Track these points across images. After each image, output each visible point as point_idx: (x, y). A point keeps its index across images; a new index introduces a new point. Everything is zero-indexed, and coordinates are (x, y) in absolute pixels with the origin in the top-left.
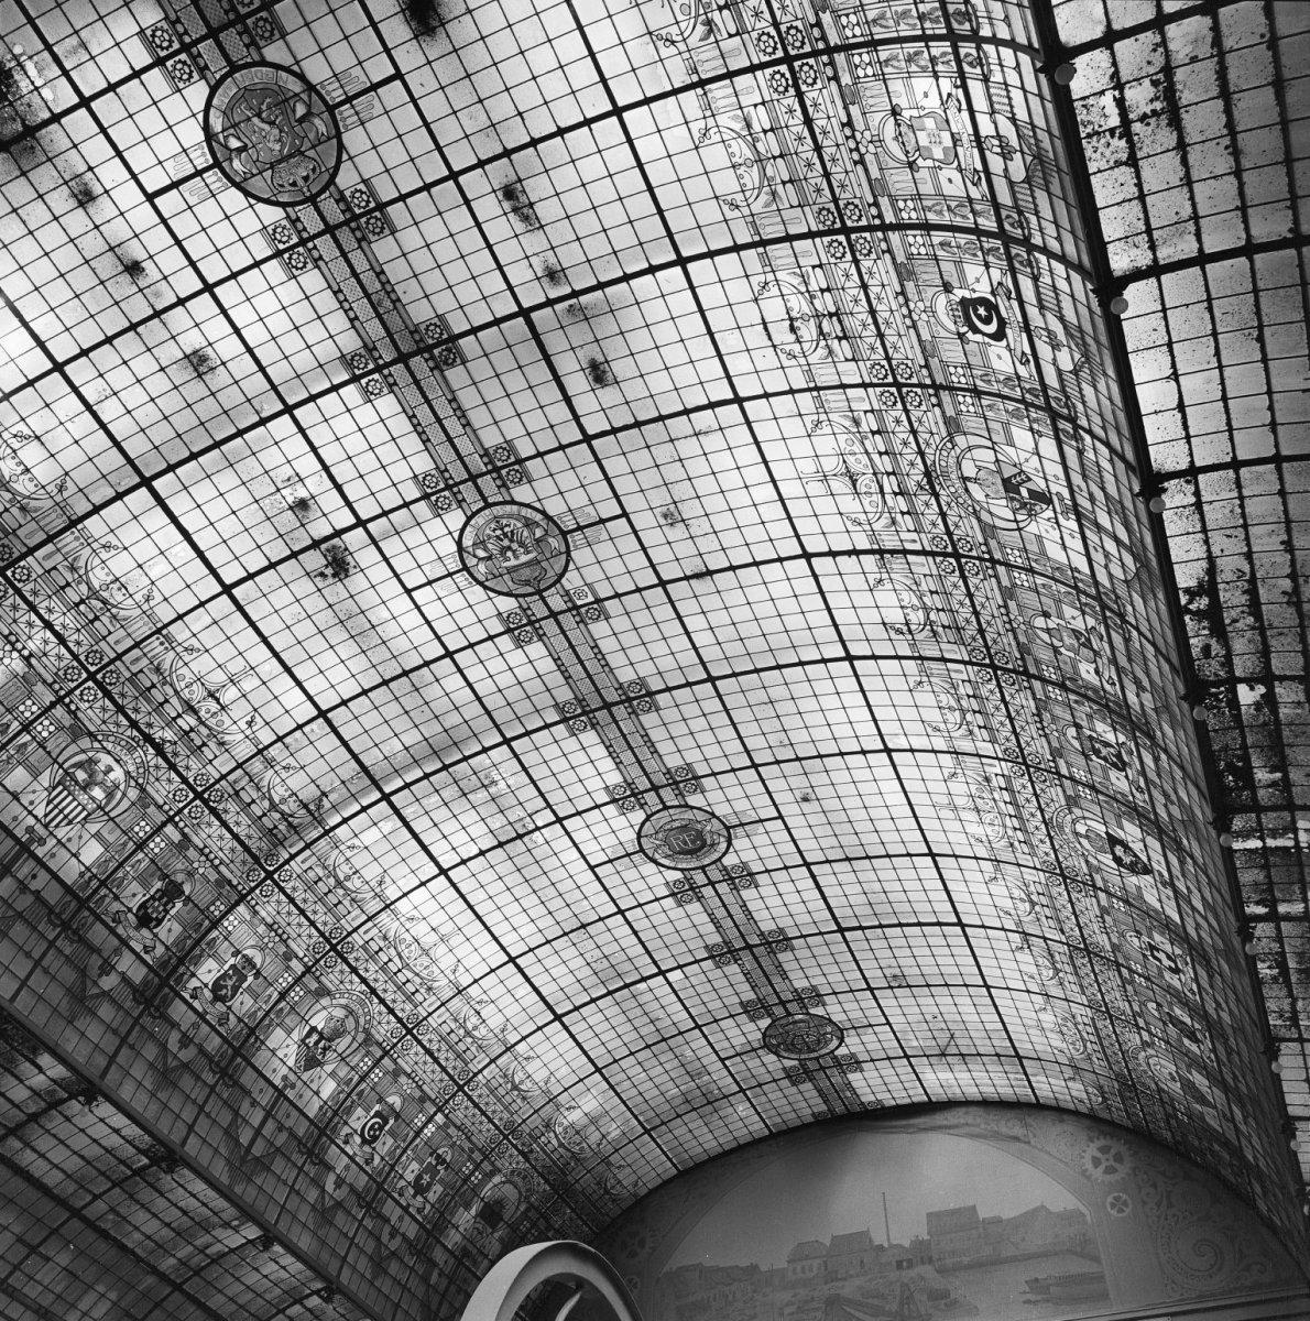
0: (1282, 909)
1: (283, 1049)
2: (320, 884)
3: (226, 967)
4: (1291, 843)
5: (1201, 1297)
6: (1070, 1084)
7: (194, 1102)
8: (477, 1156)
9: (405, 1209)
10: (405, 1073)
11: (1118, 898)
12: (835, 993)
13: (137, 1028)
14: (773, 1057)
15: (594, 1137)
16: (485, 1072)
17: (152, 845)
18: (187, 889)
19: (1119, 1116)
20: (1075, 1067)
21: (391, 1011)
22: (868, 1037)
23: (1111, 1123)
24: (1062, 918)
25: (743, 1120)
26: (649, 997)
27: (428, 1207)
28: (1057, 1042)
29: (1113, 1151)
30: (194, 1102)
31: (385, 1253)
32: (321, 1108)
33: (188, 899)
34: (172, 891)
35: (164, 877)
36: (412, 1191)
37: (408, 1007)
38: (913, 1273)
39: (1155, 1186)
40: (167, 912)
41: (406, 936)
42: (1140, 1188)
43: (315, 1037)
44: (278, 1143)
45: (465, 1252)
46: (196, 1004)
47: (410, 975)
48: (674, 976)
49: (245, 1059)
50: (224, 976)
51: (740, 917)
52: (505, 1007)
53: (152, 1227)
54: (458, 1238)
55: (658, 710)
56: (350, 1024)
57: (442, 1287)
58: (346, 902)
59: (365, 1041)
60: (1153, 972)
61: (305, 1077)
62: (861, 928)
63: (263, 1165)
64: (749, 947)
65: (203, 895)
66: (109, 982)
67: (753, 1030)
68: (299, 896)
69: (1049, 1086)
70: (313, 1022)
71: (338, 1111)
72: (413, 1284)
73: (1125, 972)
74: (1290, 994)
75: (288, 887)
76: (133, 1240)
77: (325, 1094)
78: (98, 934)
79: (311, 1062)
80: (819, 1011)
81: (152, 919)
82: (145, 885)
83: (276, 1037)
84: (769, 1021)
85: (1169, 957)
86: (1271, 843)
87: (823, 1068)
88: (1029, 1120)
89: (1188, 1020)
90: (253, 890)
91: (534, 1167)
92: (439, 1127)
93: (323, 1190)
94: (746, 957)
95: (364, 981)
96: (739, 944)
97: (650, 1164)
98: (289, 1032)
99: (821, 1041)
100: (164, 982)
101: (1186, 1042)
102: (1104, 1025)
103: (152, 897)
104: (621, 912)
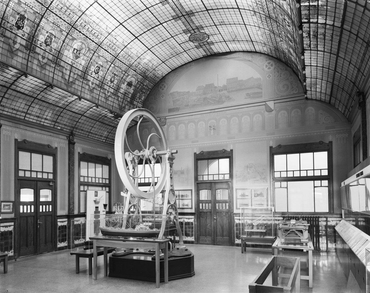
0: (311, 20)
1: (68, 55)
2: (95, 34)
3: (46, 36)
4: (316, 4)
5: (281, 96)
6: (264, 48)
7: (51, 72)
8: (124, 73)
9: (110, 86)
10: (101, 56)
11: (278, 5)
12: (206, 27)
13: (30, 57)
14: (192, 43)
15: (151, 65)
16: (121, 53)
17: (10, 5)
18: (26, 16)
19: (274, 55)
20: (265, 44)
21: (93, 41)
22: (215, 37)
23: (272, 56)
24: (264, 8)
25: (186, 58)
26: (159, 30)
27: (115, 85)
28: (261, 38)
29: (271, 64)
30: (51, 72)
31: (107, 96)
32: (83, 68)
33: (28, 19)
34: (22, 18)
35: (18, 14)
36: (110, 82)
37: (97, 40)
38: (222, 92)
39: (278, 72)
40: (24, 24)
41: (91, 21)
42: (275, 72)
43: (76, 51)
44: (75, 77)
45: (126, 93)
46: (42, 48)
47: (95, 31)
48: (165, 24)
49: (60, 59)
50: (46, 39)
51: (180, 8)
52: (122, 37)
53: (53, 98)
54: (123, 90)
55: (195, 16)
56: (84, 46)
57: (122, 101)
58: (72, 13)
59: (89, 50)
60: (284, 25)
61: (77, 61)
62: (212, 9)
63: (73, 83)
64: (183, 16)
65: (32, 18)
66: (17, 46)
67: (186, 37)
68: (58, 13)
69: (259, 48)
70: (74, 47)
71: (87, 68)
72: (115, 101)
73: (278, 24)
74: (310, 40)
75: (54, 11)
76: (50, 102)
77: (83, 64)
78: (8, 34)
79: (77, 57)
80: (203, 31)
81: (20, 27)
82: (15, 17)
83: (66, 53)
84: (190, 34)
85: (288, 22)
86: (311, 4)
87: (204, 45)
88: (253, 56)
89: (290, 37)
90: (44, 14)
91: (138, 73)
92: (113, 67)
93: (89, 86)
94: (182, 18)
95: (83, 34)
96: (180, 15)
97: (163, 70)
98: (69, 51)
99: (204, 38)
100: (31, 44)
101: (290, 42)
102: (272, 35)
103: (18, 20)
104: (147, 8)
